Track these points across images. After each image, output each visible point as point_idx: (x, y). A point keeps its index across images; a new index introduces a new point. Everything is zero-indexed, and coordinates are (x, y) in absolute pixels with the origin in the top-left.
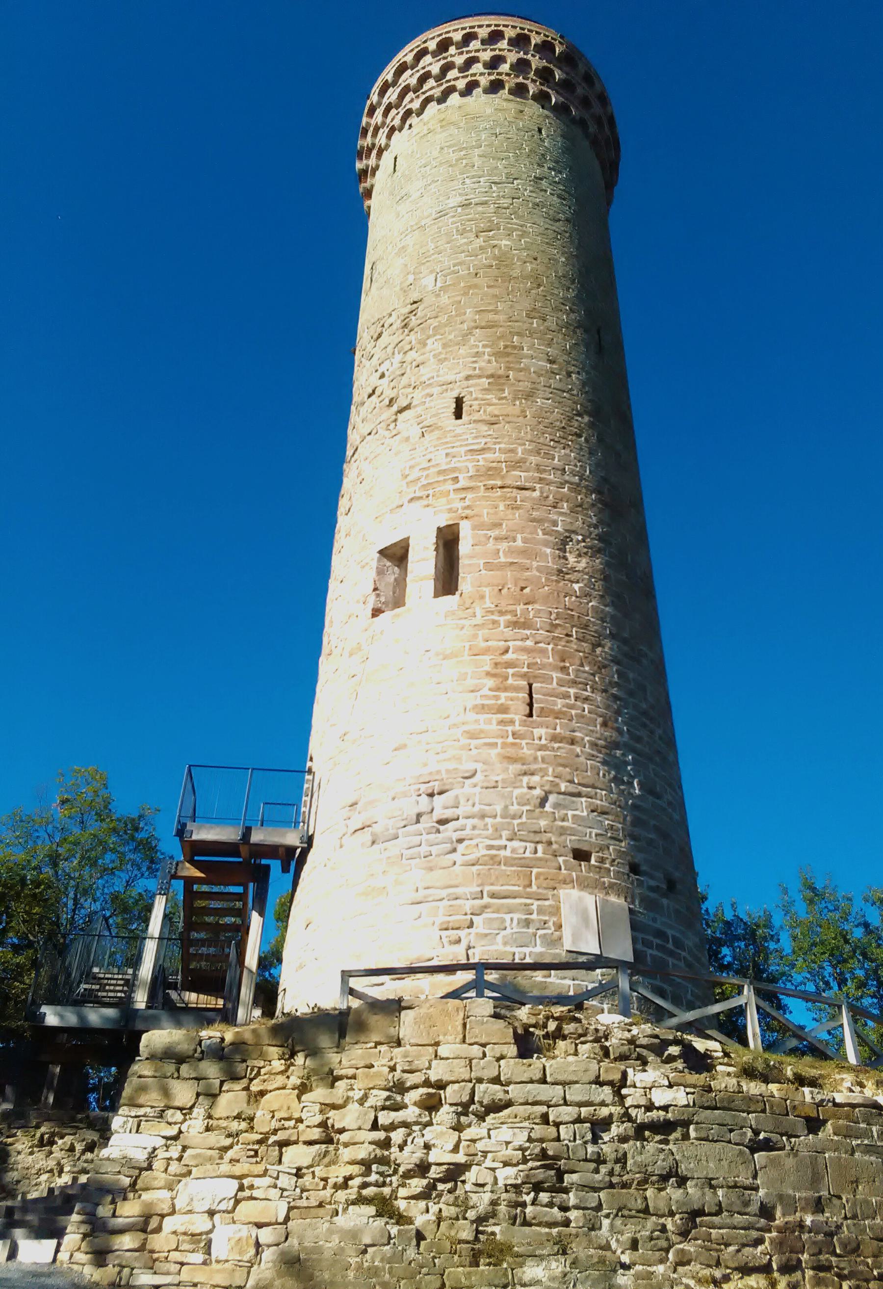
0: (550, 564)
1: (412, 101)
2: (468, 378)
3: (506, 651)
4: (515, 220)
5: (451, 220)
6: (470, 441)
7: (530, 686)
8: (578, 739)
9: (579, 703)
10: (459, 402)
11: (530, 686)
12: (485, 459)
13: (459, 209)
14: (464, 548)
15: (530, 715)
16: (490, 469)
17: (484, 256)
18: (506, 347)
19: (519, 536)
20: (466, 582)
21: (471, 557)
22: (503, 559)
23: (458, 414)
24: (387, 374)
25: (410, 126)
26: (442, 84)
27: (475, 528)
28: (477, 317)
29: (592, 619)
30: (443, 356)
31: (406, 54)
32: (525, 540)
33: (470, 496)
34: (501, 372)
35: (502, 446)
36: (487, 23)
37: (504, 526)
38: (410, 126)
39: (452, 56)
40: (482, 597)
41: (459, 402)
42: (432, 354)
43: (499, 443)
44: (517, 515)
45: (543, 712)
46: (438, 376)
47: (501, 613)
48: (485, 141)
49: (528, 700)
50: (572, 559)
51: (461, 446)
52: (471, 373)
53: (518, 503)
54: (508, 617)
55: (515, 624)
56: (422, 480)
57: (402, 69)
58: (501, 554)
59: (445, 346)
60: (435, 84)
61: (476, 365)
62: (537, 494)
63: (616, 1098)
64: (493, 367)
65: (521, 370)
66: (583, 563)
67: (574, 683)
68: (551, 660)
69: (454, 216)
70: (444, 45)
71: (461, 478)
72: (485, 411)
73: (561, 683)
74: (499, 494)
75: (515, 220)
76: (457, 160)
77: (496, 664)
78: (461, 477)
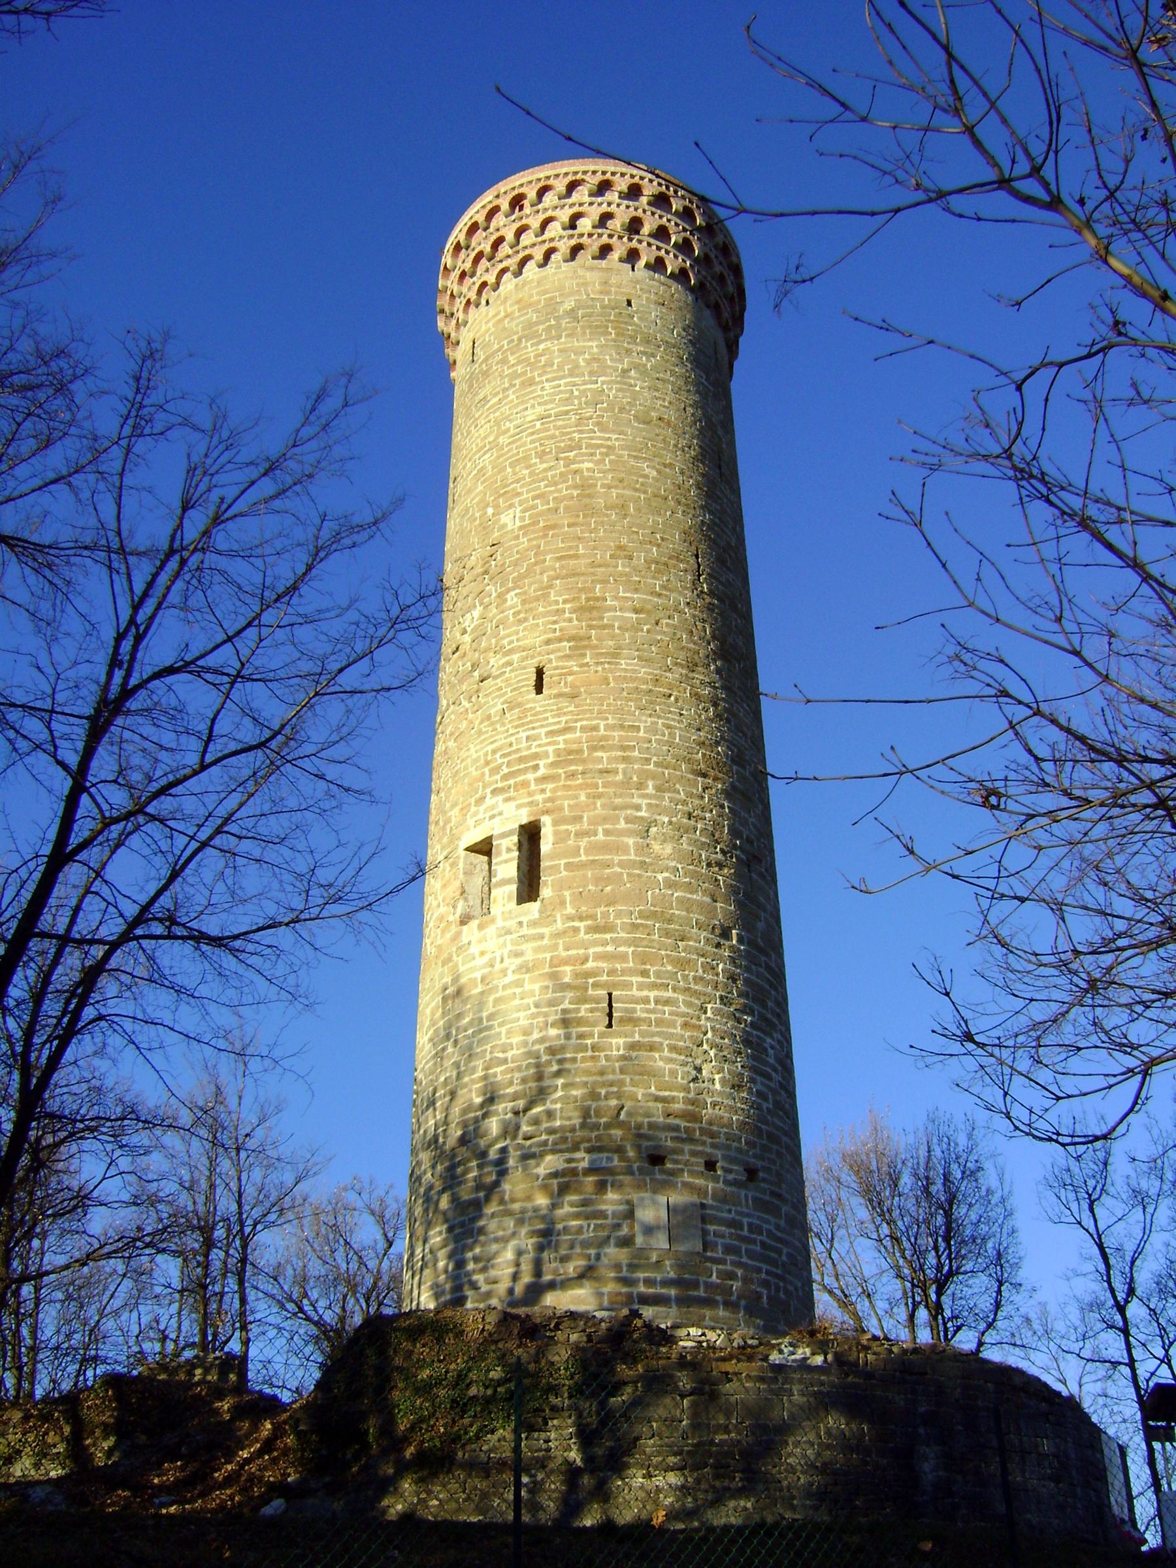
0: (633, 857)
1: (487, 270)
2: (548, 642)
3: (586, 960)
4: (598, 434)
5: (529, 439)
6: (551, 720)
7: (610, 995)
8: (657, 1045)
9: (659, 1007)
10: (540, 673)
11: (610, 995)
12: (565, 741)
13: (538, 424)
14: (546, 846)
15: (610, 1025)
16: (570, 752)
17: (564, 485)
18: (588, 600)
19: (600, 829)
20: (546, 892)
21: (552, 858)
22: (583, 858)
23: (539, 688)
24: (469, 630)
25: (487, 302)
26: (518, 252)
27: (555, 823)
28: (557, 565)
29: (677, 912)
30: (522, 615)
31: (475, 212)
32: (607, 833)
33: (550, 786)
34: (582, 632)
35: (585, 723)
36: (564, 170)
37: (585, 819)
38: (487, 302)
39: (527, 216)
40: (563, 903)
41: (540, 673)
42: (512, 612)
43: (581, 720)
44: (599, 804)
45: (622, 1021)
46: (518, 640)
47: (581, 919)
48: (566, 329)
49: (607, 1011)
50: (656, 847)
51: (542, 726)
52: (551, 635)
53: (601, 790)
54: (589, 922)
55: (596, 929)
56: (504, 767)
57: (473, 228)
58: (582, 851)
59: (524, 602)
60: (510, 252)
61: (556, 626)
62: (620, 777)
63: (38, 1028)
64: (575, 625)
65: (604, 627)
66: (669, 849)
67: (654, 986)
68: (631, 964)
69: (533, 433)
70: (517, 202)
71: (541, 766)
72: (566, 683)
73: (641, 987)
74: (580, 781)
75: (598, 434)
76: (537, 356)
77: (577, 975)
78: (541, 763)
